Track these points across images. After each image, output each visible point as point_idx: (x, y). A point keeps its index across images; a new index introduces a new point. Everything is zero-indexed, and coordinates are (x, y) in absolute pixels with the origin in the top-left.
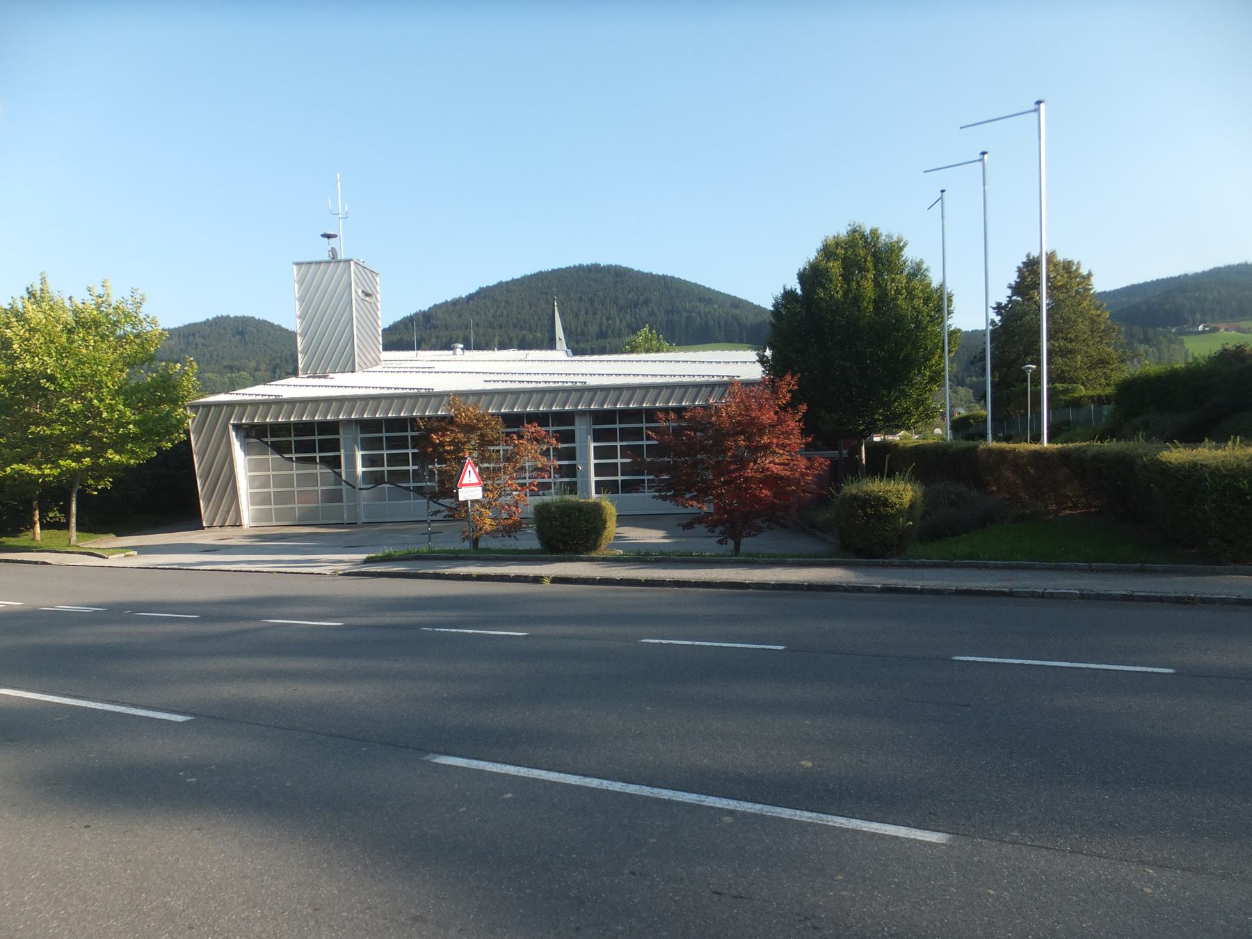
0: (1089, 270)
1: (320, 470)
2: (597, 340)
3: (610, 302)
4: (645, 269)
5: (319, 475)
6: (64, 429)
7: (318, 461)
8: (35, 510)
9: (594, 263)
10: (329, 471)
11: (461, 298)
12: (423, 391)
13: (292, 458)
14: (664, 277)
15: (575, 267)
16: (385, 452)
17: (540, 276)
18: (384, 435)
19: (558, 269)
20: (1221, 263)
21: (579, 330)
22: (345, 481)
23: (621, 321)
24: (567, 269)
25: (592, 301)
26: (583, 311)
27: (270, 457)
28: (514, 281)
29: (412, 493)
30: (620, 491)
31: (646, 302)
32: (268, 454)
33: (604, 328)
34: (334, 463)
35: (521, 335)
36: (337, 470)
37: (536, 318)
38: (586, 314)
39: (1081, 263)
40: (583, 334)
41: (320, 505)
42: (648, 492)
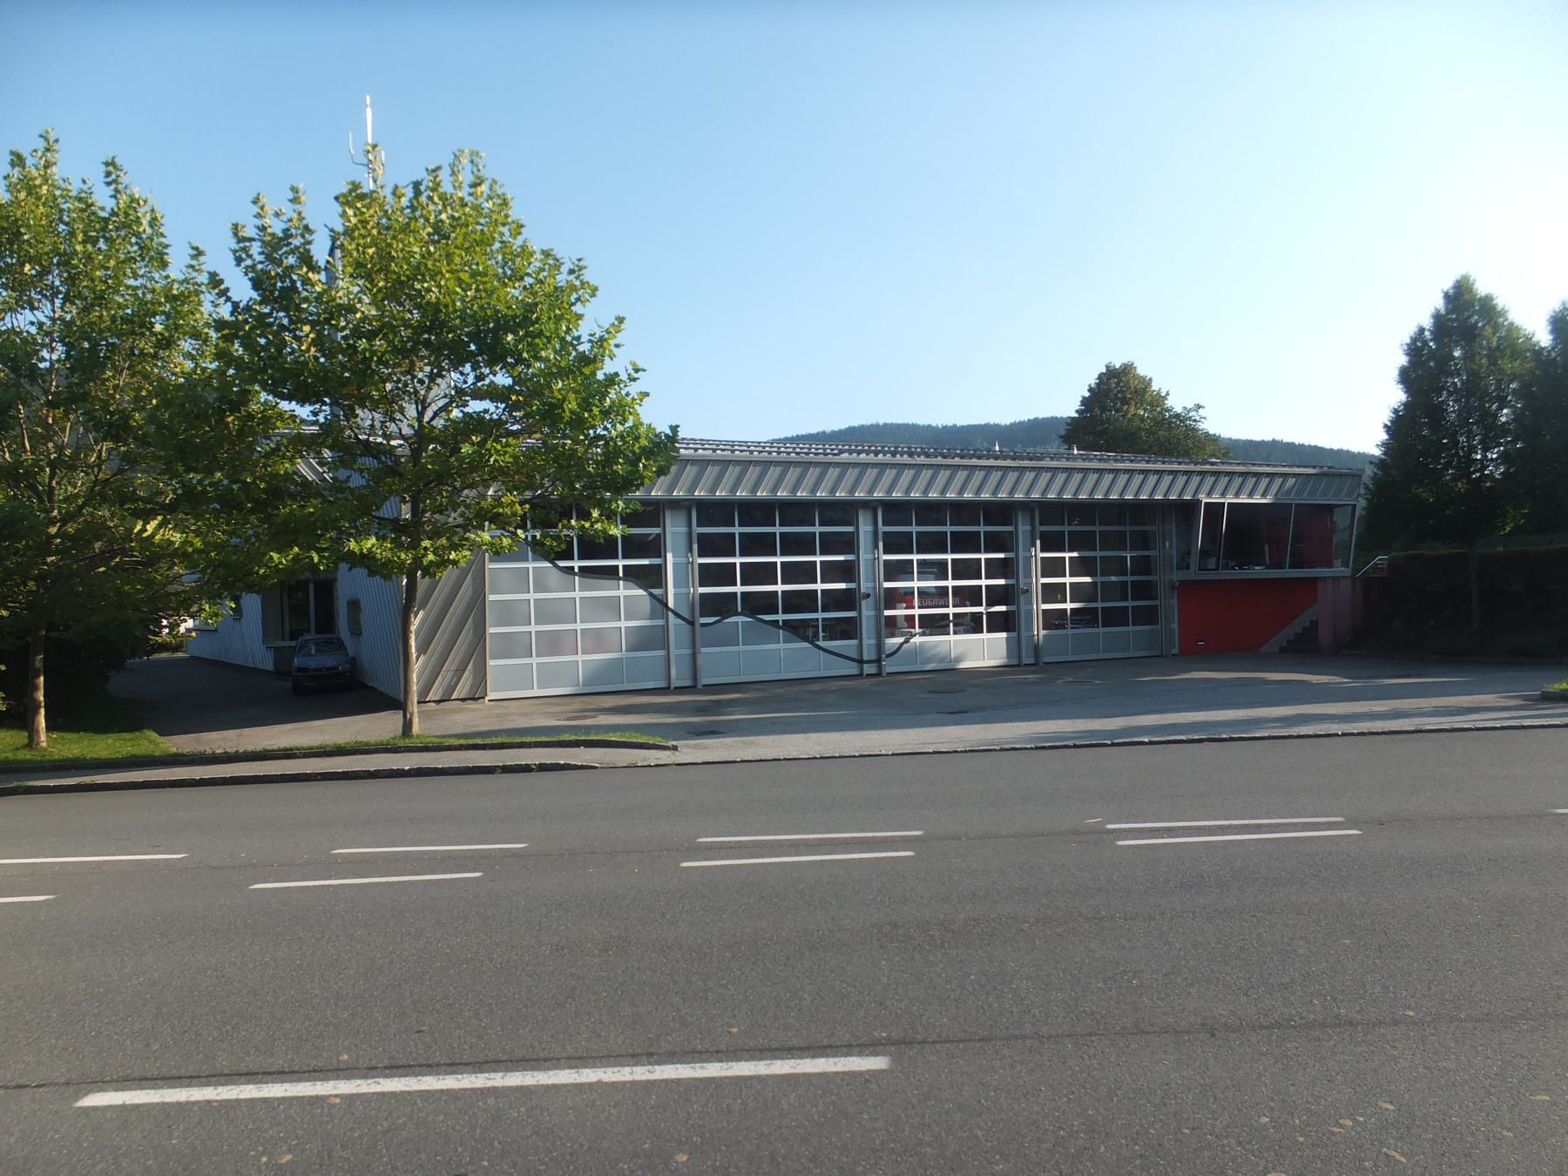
0: (255, 226)
1: (625, 591)
5: (532, 602)
7: (621, 574)
8: (38, 676)
10: (641, 592)
13: (573, 568)
22: (673, 612)
29: (781, 631)
30: (1100, 611)
32: (527, 560)
36: (656, 591)
39: (14, 150)
41: (624, 654)
42: (1072, 628)
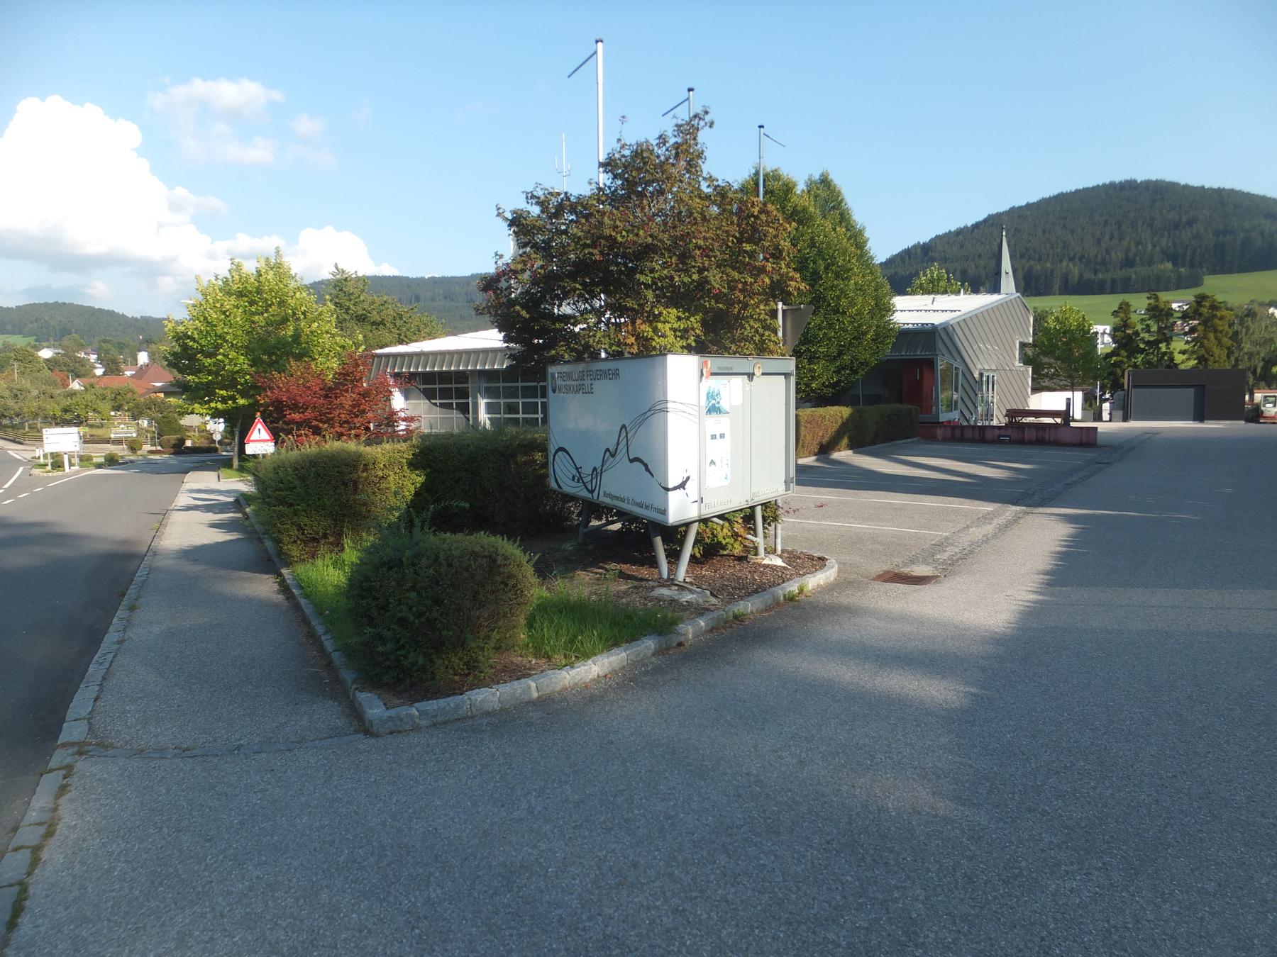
2: (1121, 269)
3: (1143, 224)
4: (1195, 181)
6: (210, 378)
9: (1129, 179)
11: (966, 227)
12: (910, 326)
14: (1219, 192)
15: (1104, 185)
16: (520, 401)
17: (1061, 199)
18: (437, 386)
19: (1083, 189)
20: (1237, 187)
21: (1100, 256)
23: (1154, 246)
24: (1093, 188)
25: (1119, 224)
26: (1107, 237)
27: (422, 402)
28: (1029, 206)
31: (1190, 223)
33: (1131, 255)
34: (464, 409)
35: (1027, 266)
37: (1048, 246)
38: (1111, 239)
40: (1104, 263)
